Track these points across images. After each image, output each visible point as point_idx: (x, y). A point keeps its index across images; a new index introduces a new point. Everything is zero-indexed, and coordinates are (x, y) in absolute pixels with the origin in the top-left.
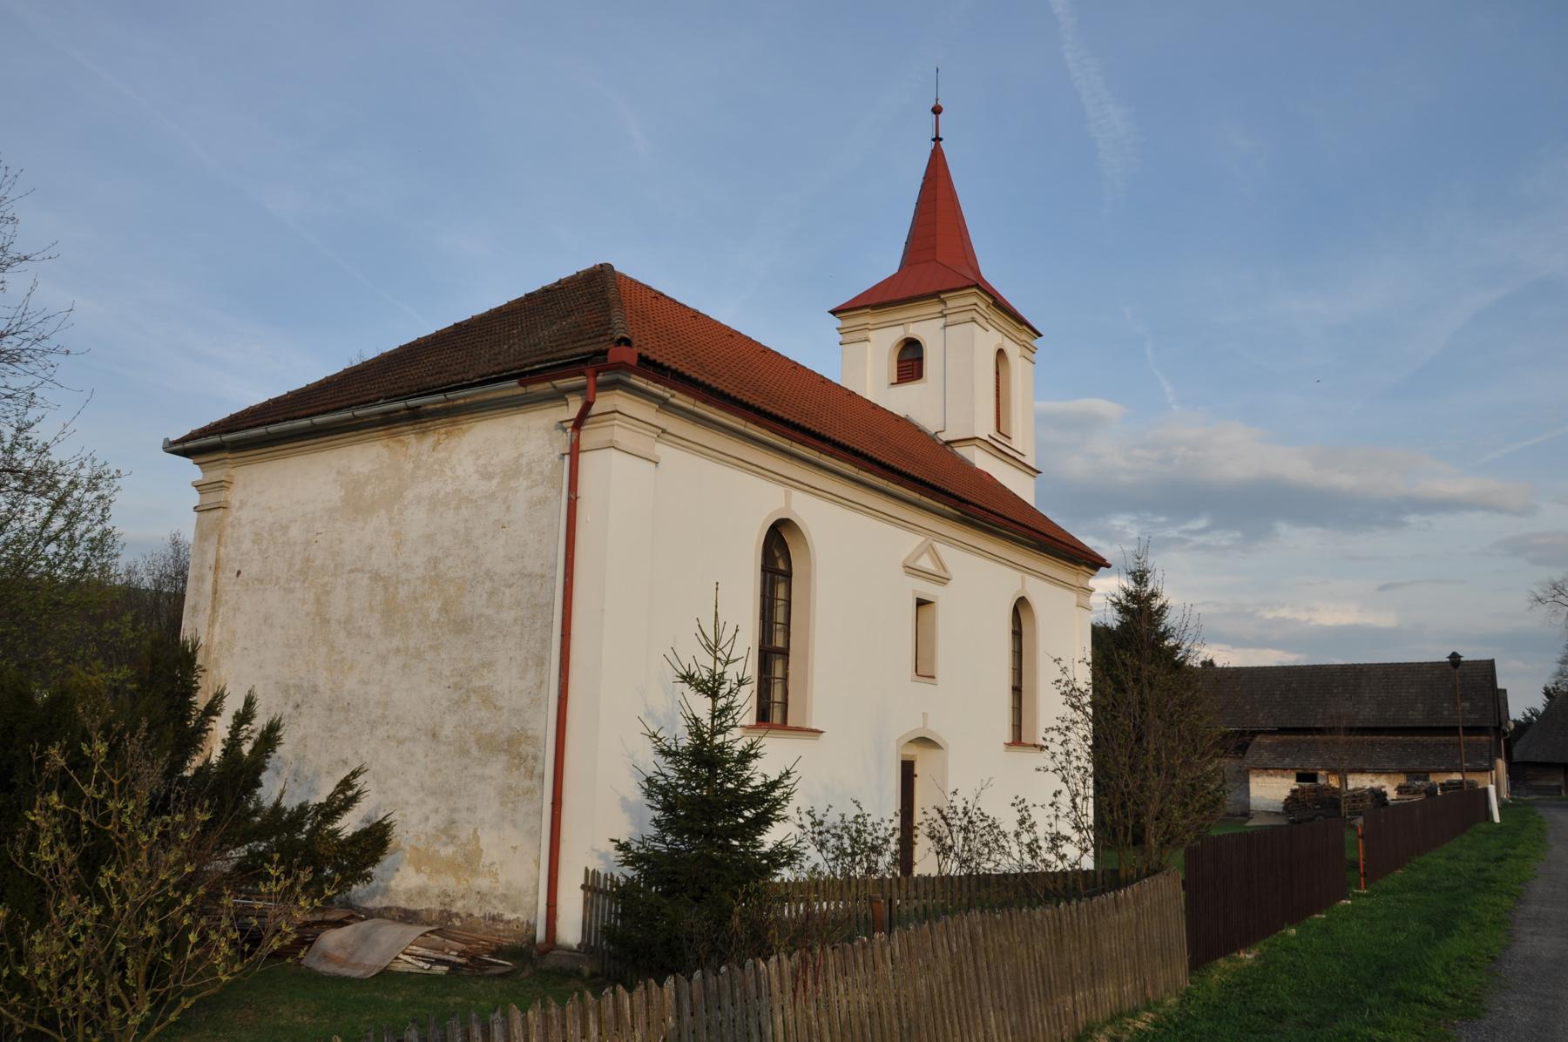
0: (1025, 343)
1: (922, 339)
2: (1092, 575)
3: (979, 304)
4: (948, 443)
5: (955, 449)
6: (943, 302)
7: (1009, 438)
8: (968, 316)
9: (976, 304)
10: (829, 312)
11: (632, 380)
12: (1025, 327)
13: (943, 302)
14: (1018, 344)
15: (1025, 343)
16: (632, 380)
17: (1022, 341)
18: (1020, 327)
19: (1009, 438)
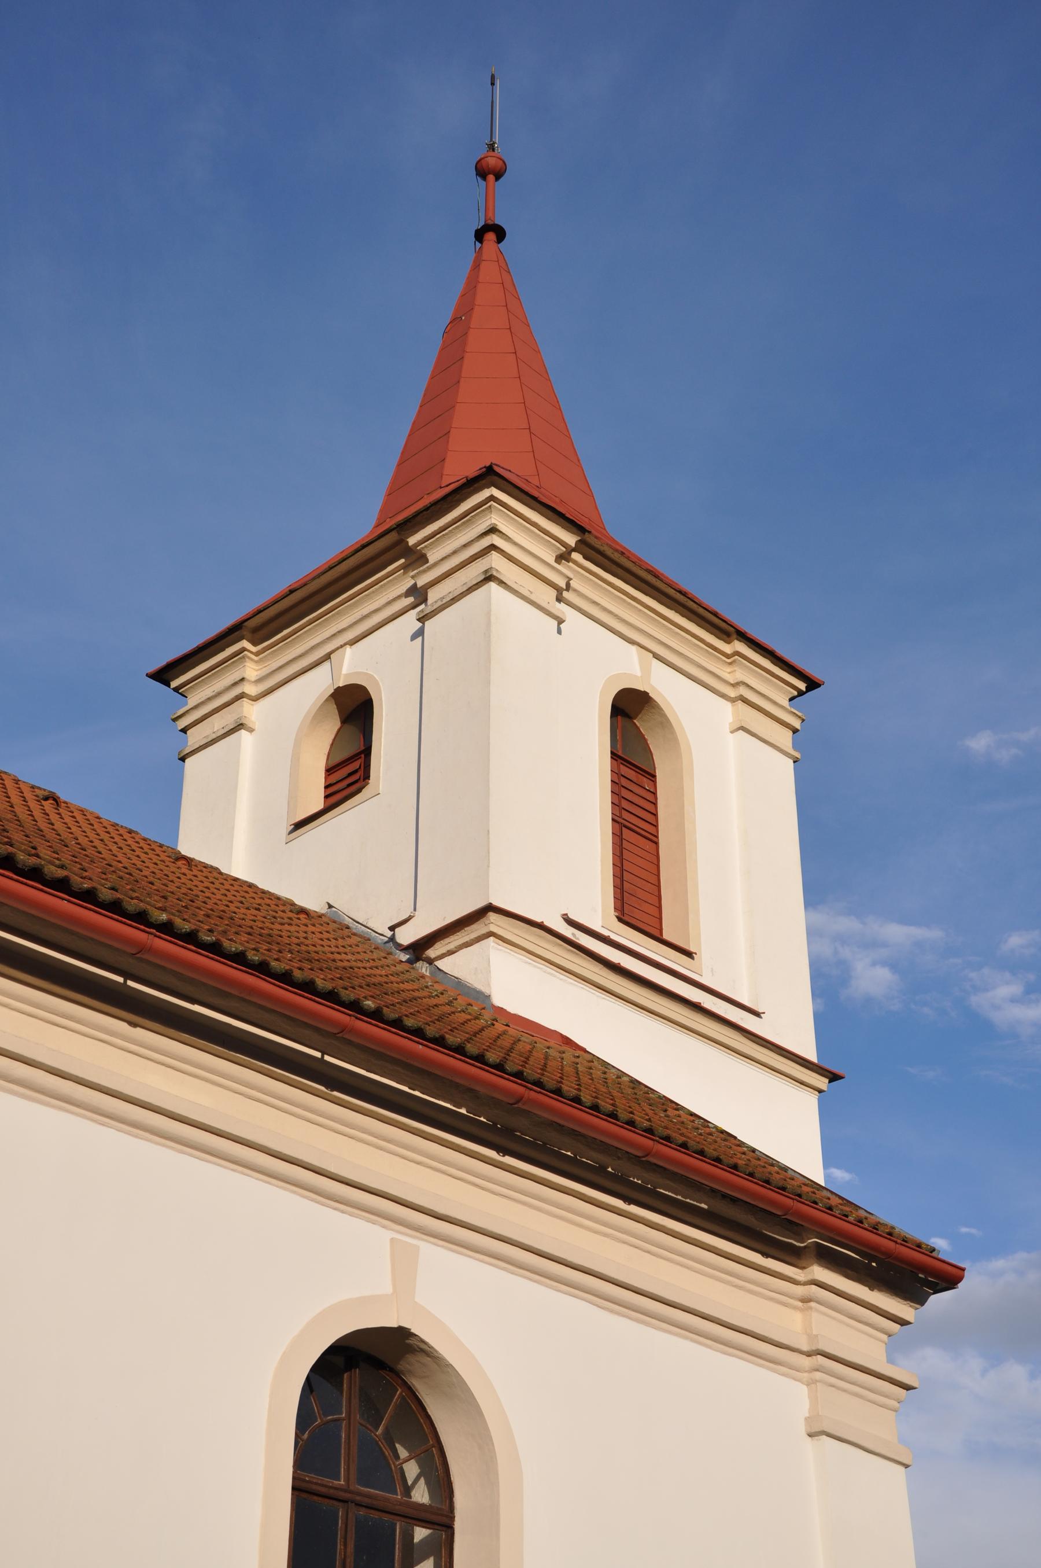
0: (743, 691)
1: (370, 677)
2: (17, 781)
3: (502, 527)
4: (419, 949)
5: (439, 964)
6: (417, 559)
7: (689, 954)
8: (474, 572)
9: (493, 530)
10: (147, 675)
11: (410, 1341)
12: (740, 646)
13: (417, 559)
14: (723, 696)
15: (743, 691)
16: (410, 1341)
17: (735, 685)
18: (727, 648)
19: (689, 954)
